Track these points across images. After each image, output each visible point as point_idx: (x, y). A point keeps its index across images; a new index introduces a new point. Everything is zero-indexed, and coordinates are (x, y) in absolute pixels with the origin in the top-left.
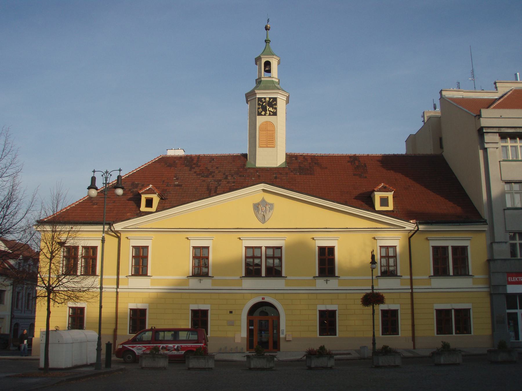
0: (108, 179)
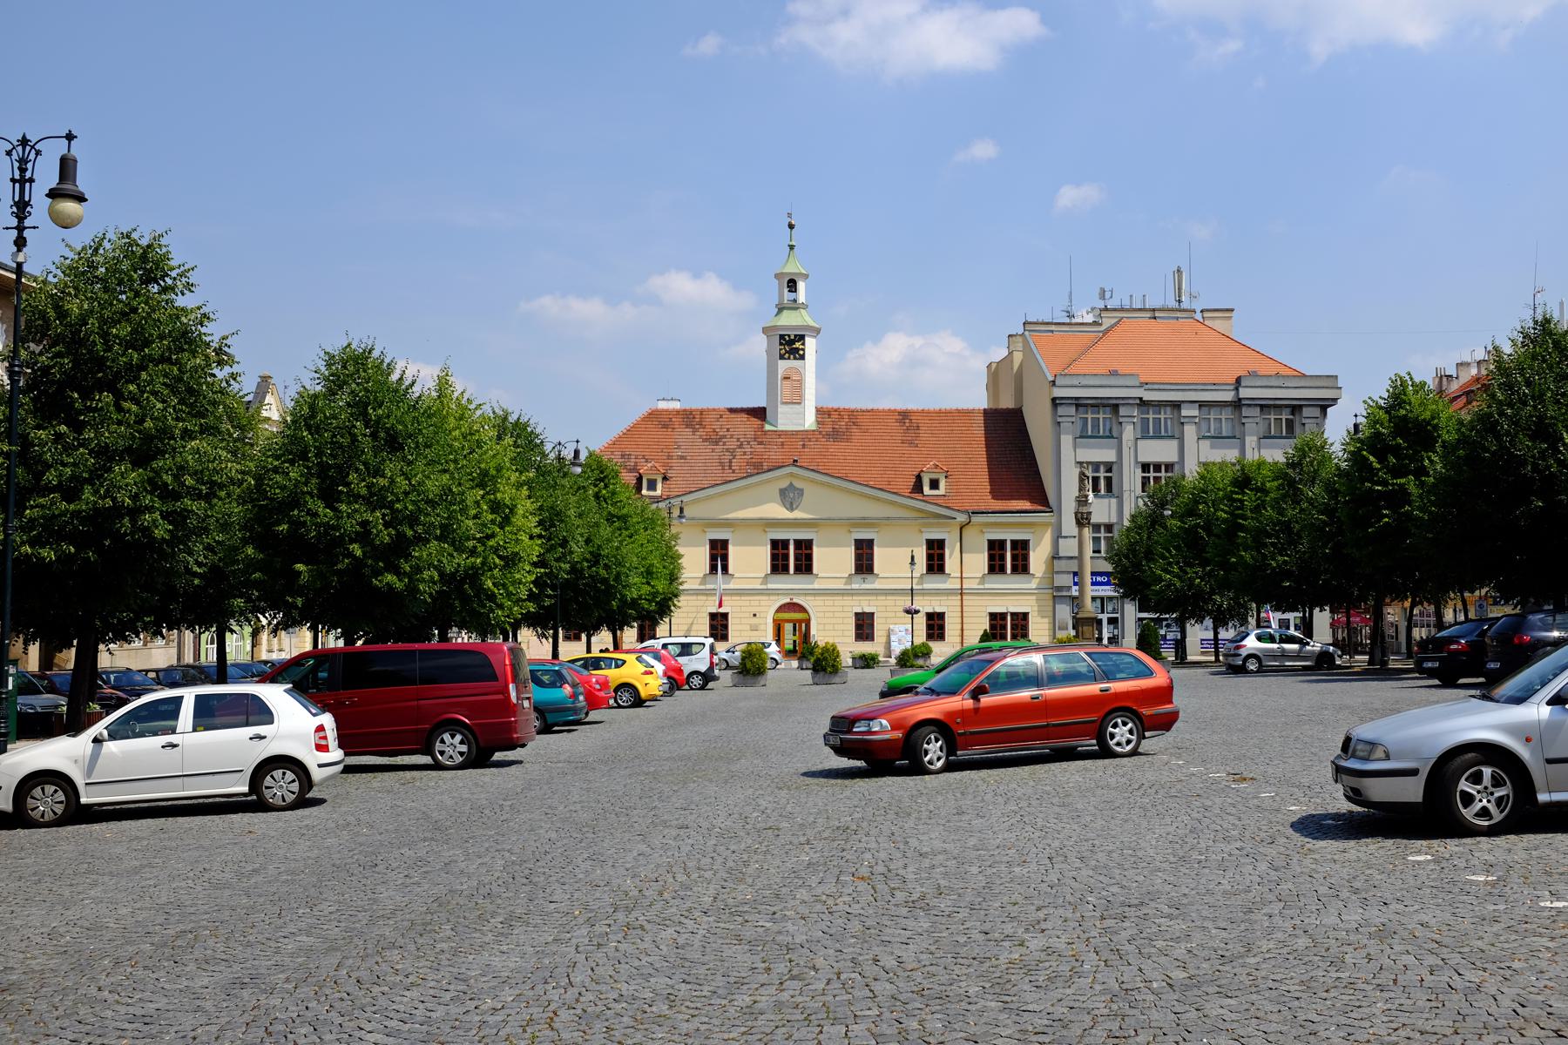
0: (29, 166)
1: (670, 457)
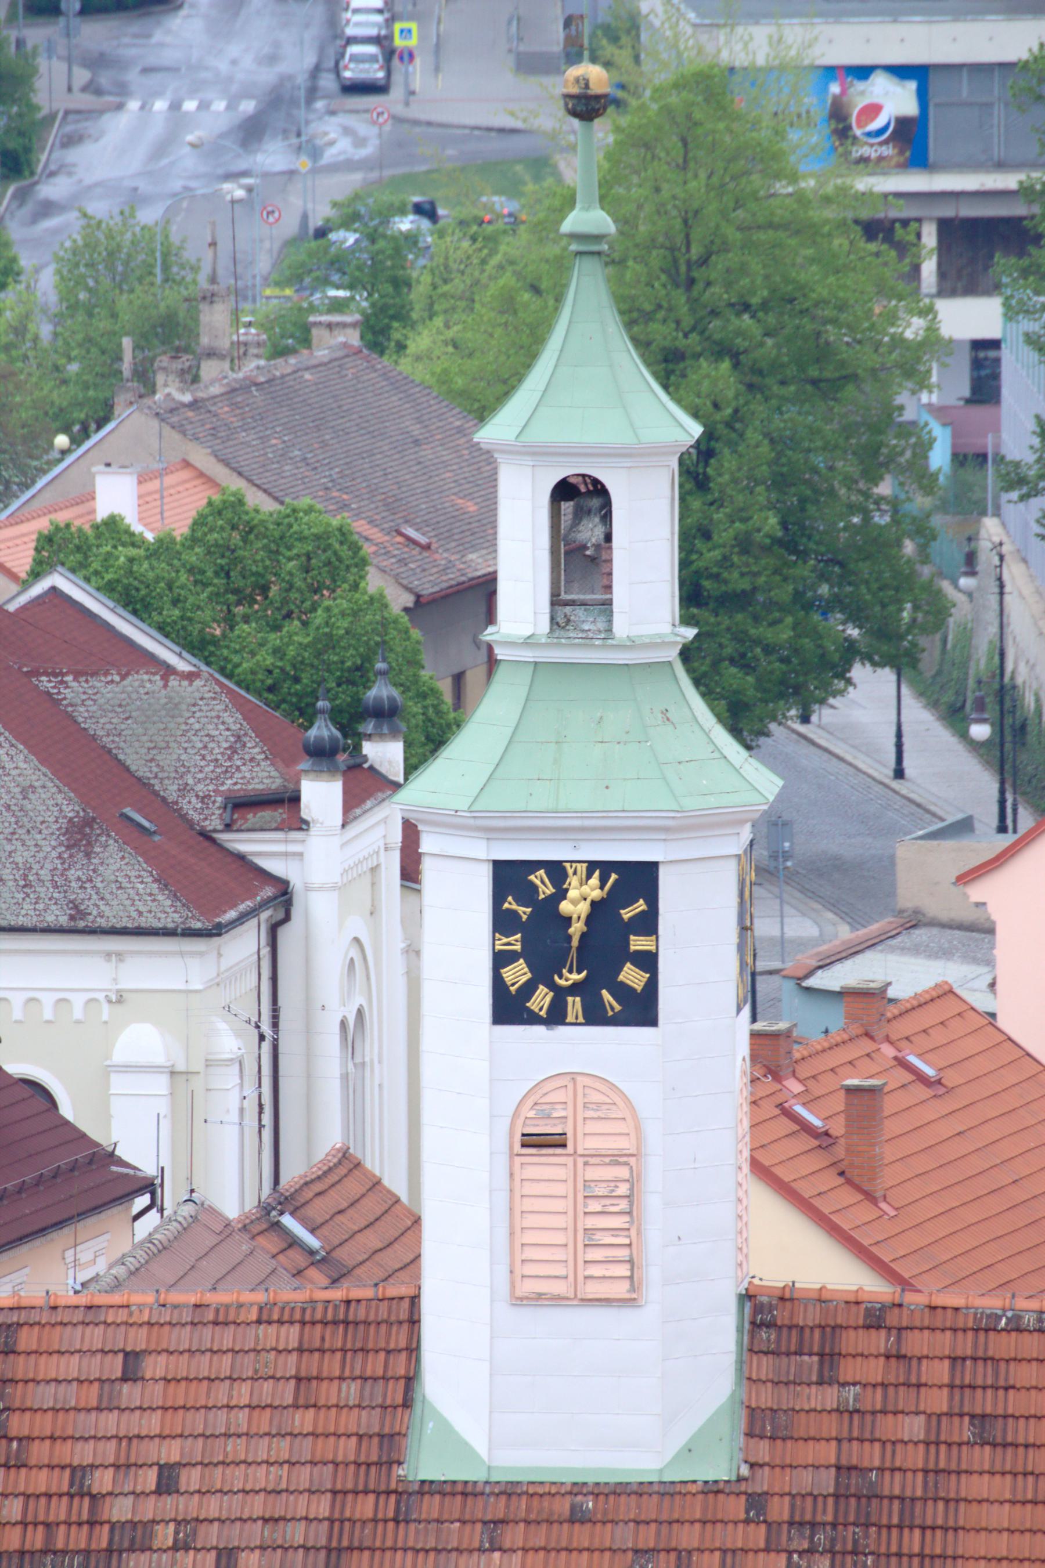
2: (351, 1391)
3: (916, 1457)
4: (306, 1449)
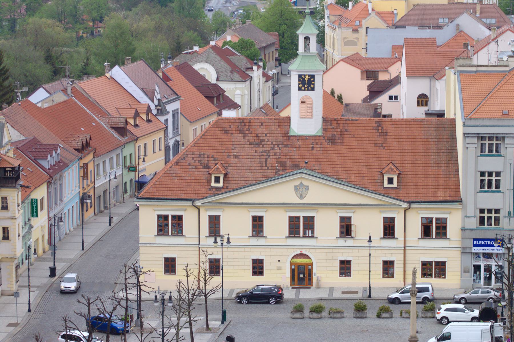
1: (229, 157)
2: (284, 127)
3: (339, 133)
4: (279, 132)
